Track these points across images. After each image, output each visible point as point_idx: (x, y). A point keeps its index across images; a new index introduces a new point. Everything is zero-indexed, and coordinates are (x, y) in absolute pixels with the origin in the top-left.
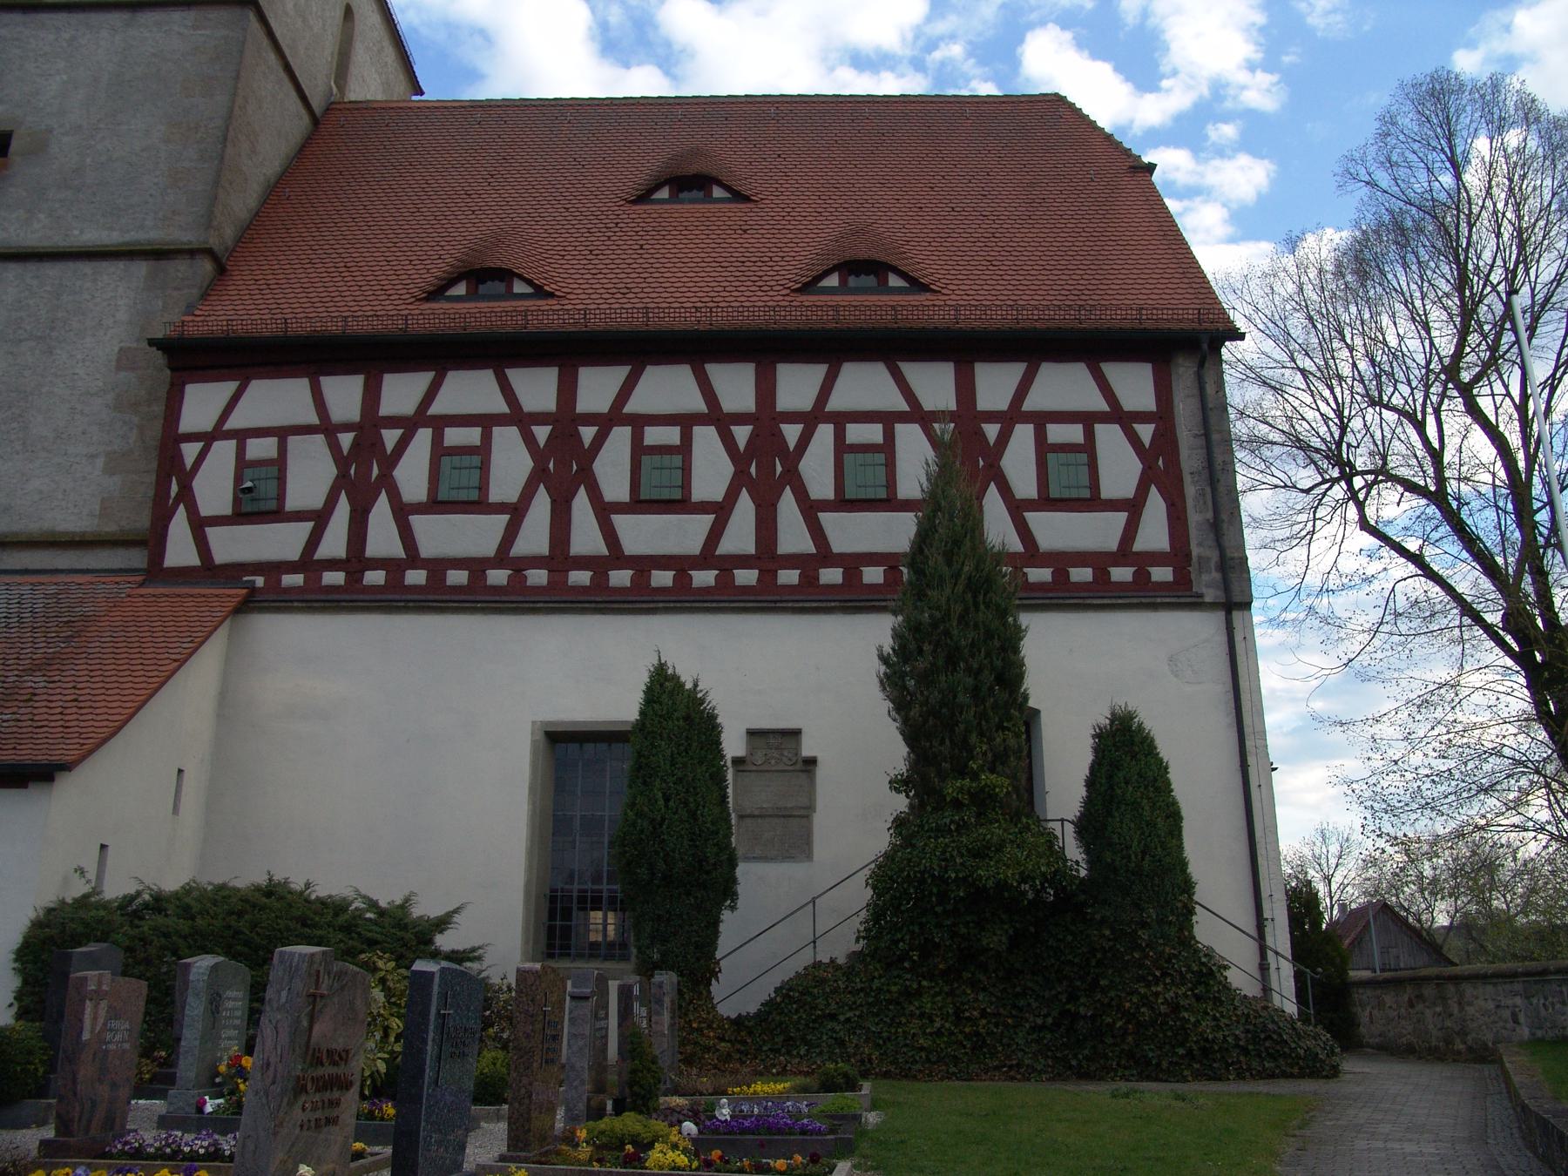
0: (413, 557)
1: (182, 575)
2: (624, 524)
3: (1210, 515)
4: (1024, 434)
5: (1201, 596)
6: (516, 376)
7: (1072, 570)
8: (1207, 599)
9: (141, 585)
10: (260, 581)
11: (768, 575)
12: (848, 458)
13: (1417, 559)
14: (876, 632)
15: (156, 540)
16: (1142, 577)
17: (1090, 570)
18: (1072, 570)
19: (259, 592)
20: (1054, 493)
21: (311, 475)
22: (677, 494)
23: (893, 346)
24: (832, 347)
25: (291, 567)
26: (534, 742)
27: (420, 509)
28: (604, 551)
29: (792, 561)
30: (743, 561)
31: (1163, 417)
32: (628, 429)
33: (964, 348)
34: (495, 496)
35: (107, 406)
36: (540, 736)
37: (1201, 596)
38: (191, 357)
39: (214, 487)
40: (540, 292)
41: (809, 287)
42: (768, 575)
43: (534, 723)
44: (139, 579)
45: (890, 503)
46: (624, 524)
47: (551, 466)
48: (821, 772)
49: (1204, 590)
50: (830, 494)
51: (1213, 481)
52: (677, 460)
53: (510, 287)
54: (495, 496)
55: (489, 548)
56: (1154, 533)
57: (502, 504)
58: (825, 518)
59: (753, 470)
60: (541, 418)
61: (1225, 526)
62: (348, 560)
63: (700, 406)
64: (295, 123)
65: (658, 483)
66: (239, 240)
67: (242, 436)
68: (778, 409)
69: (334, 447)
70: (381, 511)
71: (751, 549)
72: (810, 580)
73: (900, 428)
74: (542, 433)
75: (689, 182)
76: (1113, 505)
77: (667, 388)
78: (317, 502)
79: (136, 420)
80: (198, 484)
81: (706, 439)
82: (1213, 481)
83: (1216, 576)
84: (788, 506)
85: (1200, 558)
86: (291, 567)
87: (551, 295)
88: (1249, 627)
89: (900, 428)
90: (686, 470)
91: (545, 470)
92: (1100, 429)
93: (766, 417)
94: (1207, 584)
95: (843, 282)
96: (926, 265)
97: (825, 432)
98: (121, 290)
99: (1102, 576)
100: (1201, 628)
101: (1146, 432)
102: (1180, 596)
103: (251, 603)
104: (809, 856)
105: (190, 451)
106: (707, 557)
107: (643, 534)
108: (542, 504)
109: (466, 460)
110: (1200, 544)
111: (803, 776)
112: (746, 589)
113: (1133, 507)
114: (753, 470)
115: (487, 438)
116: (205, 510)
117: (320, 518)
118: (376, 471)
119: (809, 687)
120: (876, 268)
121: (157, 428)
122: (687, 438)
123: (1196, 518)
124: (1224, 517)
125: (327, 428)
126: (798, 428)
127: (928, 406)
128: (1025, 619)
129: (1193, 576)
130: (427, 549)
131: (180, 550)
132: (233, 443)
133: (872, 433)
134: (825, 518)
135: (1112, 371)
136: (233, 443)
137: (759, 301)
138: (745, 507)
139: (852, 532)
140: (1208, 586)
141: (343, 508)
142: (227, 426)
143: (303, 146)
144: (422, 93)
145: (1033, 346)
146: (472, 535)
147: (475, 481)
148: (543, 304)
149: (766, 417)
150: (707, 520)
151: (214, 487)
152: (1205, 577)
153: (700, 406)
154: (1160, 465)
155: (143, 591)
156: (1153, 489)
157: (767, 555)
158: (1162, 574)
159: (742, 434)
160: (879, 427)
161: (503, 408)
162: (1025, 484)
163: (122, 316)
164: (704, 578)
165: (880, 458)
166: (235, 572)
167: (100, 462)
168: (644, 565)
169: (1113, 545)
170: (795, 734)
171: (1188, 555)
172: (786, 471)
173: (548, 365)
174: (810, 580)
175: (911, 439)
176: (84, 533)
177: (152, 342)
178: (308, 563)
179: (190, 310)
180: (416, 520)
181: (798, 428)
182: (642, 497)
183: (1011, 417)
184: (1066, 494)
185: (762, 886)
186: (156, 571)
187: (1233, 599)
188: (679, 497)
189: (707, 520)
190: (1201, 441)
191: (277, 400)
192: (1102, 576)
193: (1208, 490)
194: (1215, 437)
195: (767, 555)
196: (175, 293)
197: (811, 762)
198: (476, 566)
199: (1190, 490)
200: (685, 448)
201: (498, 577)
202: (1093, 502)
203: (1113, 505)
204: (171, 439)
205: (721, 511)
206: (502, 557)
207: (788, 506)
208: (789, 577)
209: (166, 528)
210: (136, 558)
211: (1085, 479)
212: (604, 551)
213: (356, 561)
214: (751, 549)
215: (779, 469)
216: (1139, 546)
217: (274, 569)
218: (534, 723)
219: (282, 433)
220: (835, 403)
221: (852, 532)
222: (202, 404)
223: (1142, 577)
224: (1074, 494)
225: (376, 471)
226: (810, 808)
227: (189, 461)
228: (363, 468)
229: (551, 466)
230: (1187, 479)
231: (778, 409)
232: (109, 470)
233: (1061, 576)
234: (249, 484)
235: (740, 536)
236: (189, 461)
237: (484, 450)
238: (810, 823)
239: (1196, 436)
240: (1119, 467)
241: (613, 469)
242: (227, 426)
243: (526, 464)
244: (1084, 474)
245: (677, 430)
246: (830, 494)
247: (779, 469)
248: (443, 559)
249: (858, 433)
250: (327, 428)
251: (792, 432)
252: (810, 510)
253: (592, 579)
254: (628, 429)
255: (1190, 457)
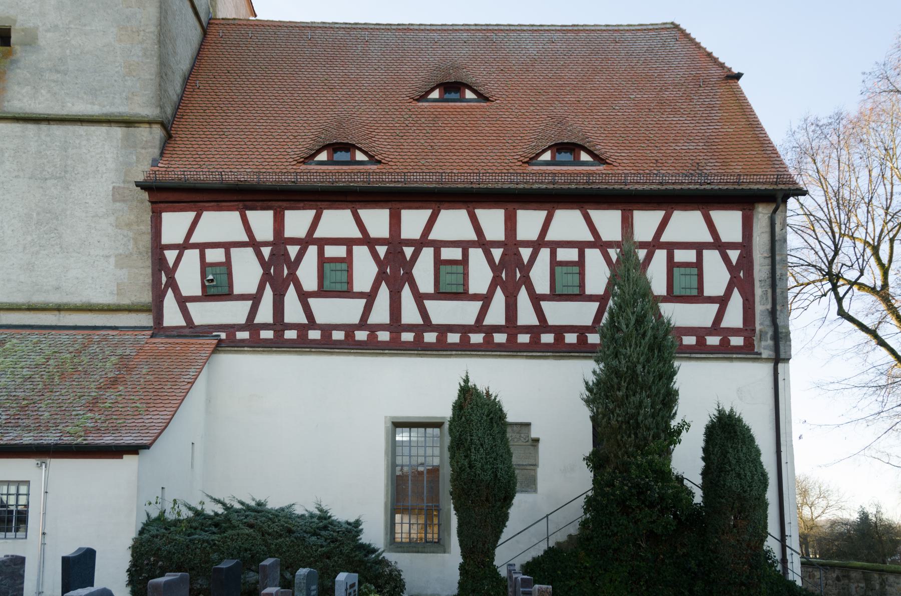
0: (312, 323)
1: (175, 332)
2: (547, 306)
3: (769, 306)
4: (427, 254)
5: (760, 354)
6: (364, 213)
7: (731, 338)
8: (764, 356)
9: (152, 337)
10: (223, 336)
11: (512, 338)
12: (558, 269)
13: (873, 333)
14: (583, 371)
15: (156, 308)
16: (725, 342)
17: (694, 338)
18: (731, 338)
19: (226, 340)
20: (677, 291)
21: (247, 272)
22: (461, 290)
23: (585, 199)
24: (550, 199)
25: (241, 328)
26: (386, 428)
27: (429, 297)
28: (421, 322)
29: (410, 328)
30: (497, 329)
31: (746, 246)
32: (665, 252)
33: (627, 200)
34: (357, 288)
35: (111, 224)
36: (389, 424)
37: (760, 354)
38: (164, 194)
39: (189, 278)
40: (373, 160)
41: (309, 158)
42: (512, 338)
43: (386, 417)
44: (150, 332)
45: (581, 296)
46: (547, 306)
47: (388, 270)
48: (541, 445)
49: (762, 351)
50: (547, 291)
51: (773, 286)
52: (460, 268)
53: (354, 155)
54: (357, 288)
55: (471, 320)
56: (734, 317)
57: (362, 293)
58: (428, 304)
59: (503, 275)
60: (381, 241)
61: (778, 313)
62: (390, 325)
63: (473, 236)
64: (194, 33)
65: (450, 280)
66: (174, 116)
67: (202, 247)
68: (518, 239)
69: (726, 259)
70: (291, 296)
71: (502, 322)
72: (535, 340)
73: (356, 249)
74: (382, 250)
75: (452, 87)
76: (711, 300)
77: (453, 224)
78: (253, 289)
79: (131, 234)
80: (179, 276)
81: (476, 256)
82: (773, 286)
83: (770, 343)
84: (523, 297)
85: (761, 331)
86: (241, 328)
87: (379, 162)
88: (787, 373)
89: (356, 249)
90: (466, 275)
91: (385, 273)
92: (706, 253)
93: (511, 243)
94: (765, 347)
95: (553, 157)
96: (382, 146)
97: (545, 253)
98: (106, 147)
99: (701, 341)
100: (761, 371)
101: (734, 255)
102: (748, 352)
103: (220, 347)
104: (535, 491)
105: (171, 256)
106: (478, 326)
107: (443, 312)
108: (384, 292)
109: (454, 268)
110: (761, 324)
111: (532, 448)
112: (314, 341)
113: (723, 301)
114: (503, 275)
115: (350, 252)
116: (185, 293)
117: (256, 299)
118: (286, 272)
119: (549, 403)
120: (573, 148)
121: (146, 240)
122: (465, 255)
123: (761, 307)
124: (778, 308)
125: (254, 244)
126: (297, 248)
127: (724, 238)
128: (676, 364)
129: (755, 343)
130: (320, 319)
131: (172, 316)
132: (197, 251)
133: (688, 256)
134: (428, 304)
135: (596, 215)
136: (197, 251)
137: (277, 167)
138: (499, 298)
139: (559, 313)
140: (764, 349)
141: (268, 293)
142: (192, 241)
143: (199, 50)
144: (256, 16)
145: (669, 200)
146: (346, 311)
147: (577, 282)
148: (601, 168)
149: (511, 243)
150: (478, 304)
151: (189, 278)
152: (763, 343)
153: (473, 236)
154: (741, 277)
155: (153, 340)
156: (736, 290)
157: (511, 325)
158: (737, 341)
159: (497, 253)
160: (460, 250)
161: (710, 239)
162: (542, 286)
163: (111, 165)
164: (713, 341)
165: (576, 269)
166: (207, 331)
167: (112, 260)
168: (443, 330)
169: (709, 324)
170: (528, 425)
171: (754, 330)
172: (405, 273)
173: (383, 208)
174: (535, 340)
175: (593, 256)
176: (109, 305)
177: (138, 184)
178: (250, 325)
179: (155, 163)
180: (312, 301)
181: (297, 248)
182: (441, 291)
183: (654, 244)
184: (683, 293)
185: (522, 507)
186: (158, 329)
187: (779, 356)
188: (461, 291)
189: (478, 304)
190: (768, 261)
191: (220, 224)
192: (701, 341)
193: (770, 291)
194: (778, 258)
195: (511, 325)
196: (143, 151)
197: (537, 441)
198: (350, 329)
199: (758, 291)
200: (465, 261)
201: (361, 335)
202: (699, 298)
203: (711, 300)
204: (158, 249)
205: (486, 300)
206: (363, 324)
207: (523, 297)
208: (524, 338)
209: (162, 301)
210: (146, 320)
211: (695, 284)
212: (421, 322)
213: (279, 324)
214: (502, 322)
215: (518, 275)
216: (724, 324)
217: (231, 329)
218: (386, 417)
219: (227, 246)
220: (435, 234)
221: (559, 313)
222: (174, 225)
223: (725, 342)
224: (688, 293)
225: (286, 272)
226: (536, 465)
227: (171, 263)
228: (278, 271)
229: (388, 270)
230: (757, 284)
231: (518, 239)
232: (119, 265)
233: (442, 338)
234: (211, 277)
235: (496, 315)
236: (171, 263)
237: (348, 260)
238: (536, 473)
239: (765, 258)
240: (716, 277)
241: (424, 273)
242: (192, 241)
243: (374, 269)
244: (695, 279)
245: (694, 252)
246: (547, 291)
247: (518, 275)
248: (329, 325)
249: (331, 251)
250: (254, 244)
251: (293, 251)
252: (536, 300)
253: (484, 338)
254: (665, 252)
255: (760, 270)
